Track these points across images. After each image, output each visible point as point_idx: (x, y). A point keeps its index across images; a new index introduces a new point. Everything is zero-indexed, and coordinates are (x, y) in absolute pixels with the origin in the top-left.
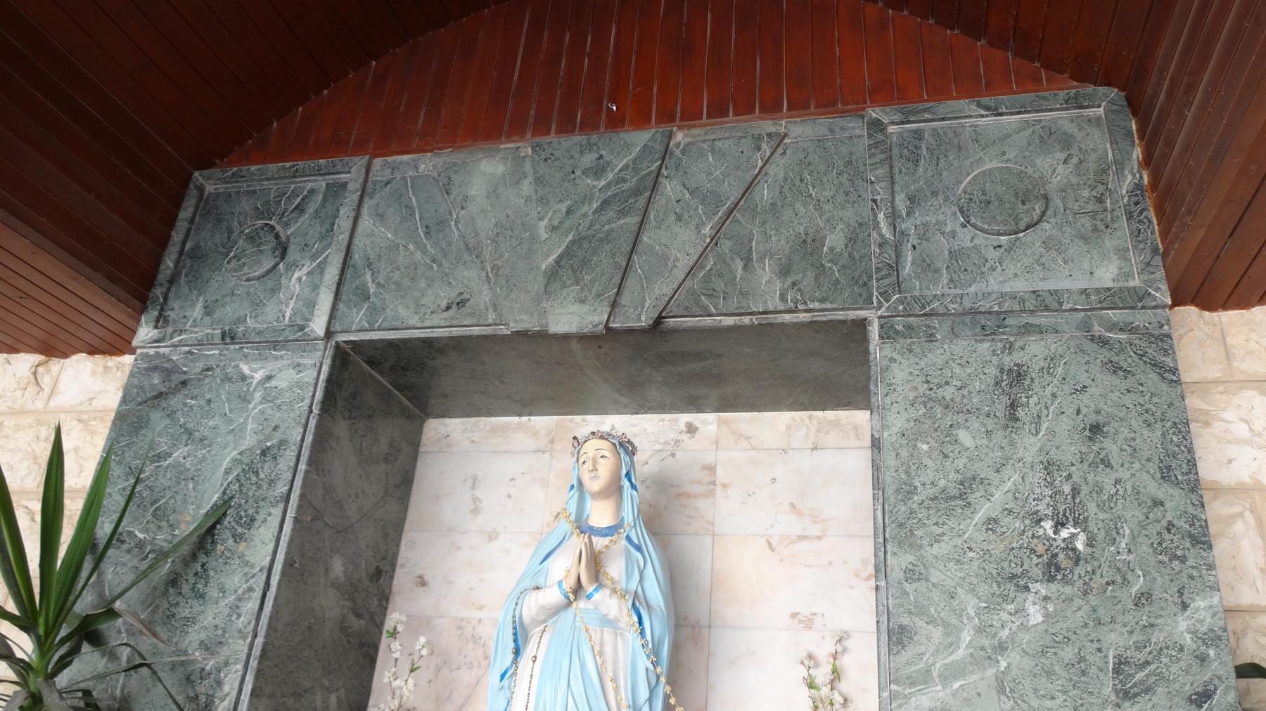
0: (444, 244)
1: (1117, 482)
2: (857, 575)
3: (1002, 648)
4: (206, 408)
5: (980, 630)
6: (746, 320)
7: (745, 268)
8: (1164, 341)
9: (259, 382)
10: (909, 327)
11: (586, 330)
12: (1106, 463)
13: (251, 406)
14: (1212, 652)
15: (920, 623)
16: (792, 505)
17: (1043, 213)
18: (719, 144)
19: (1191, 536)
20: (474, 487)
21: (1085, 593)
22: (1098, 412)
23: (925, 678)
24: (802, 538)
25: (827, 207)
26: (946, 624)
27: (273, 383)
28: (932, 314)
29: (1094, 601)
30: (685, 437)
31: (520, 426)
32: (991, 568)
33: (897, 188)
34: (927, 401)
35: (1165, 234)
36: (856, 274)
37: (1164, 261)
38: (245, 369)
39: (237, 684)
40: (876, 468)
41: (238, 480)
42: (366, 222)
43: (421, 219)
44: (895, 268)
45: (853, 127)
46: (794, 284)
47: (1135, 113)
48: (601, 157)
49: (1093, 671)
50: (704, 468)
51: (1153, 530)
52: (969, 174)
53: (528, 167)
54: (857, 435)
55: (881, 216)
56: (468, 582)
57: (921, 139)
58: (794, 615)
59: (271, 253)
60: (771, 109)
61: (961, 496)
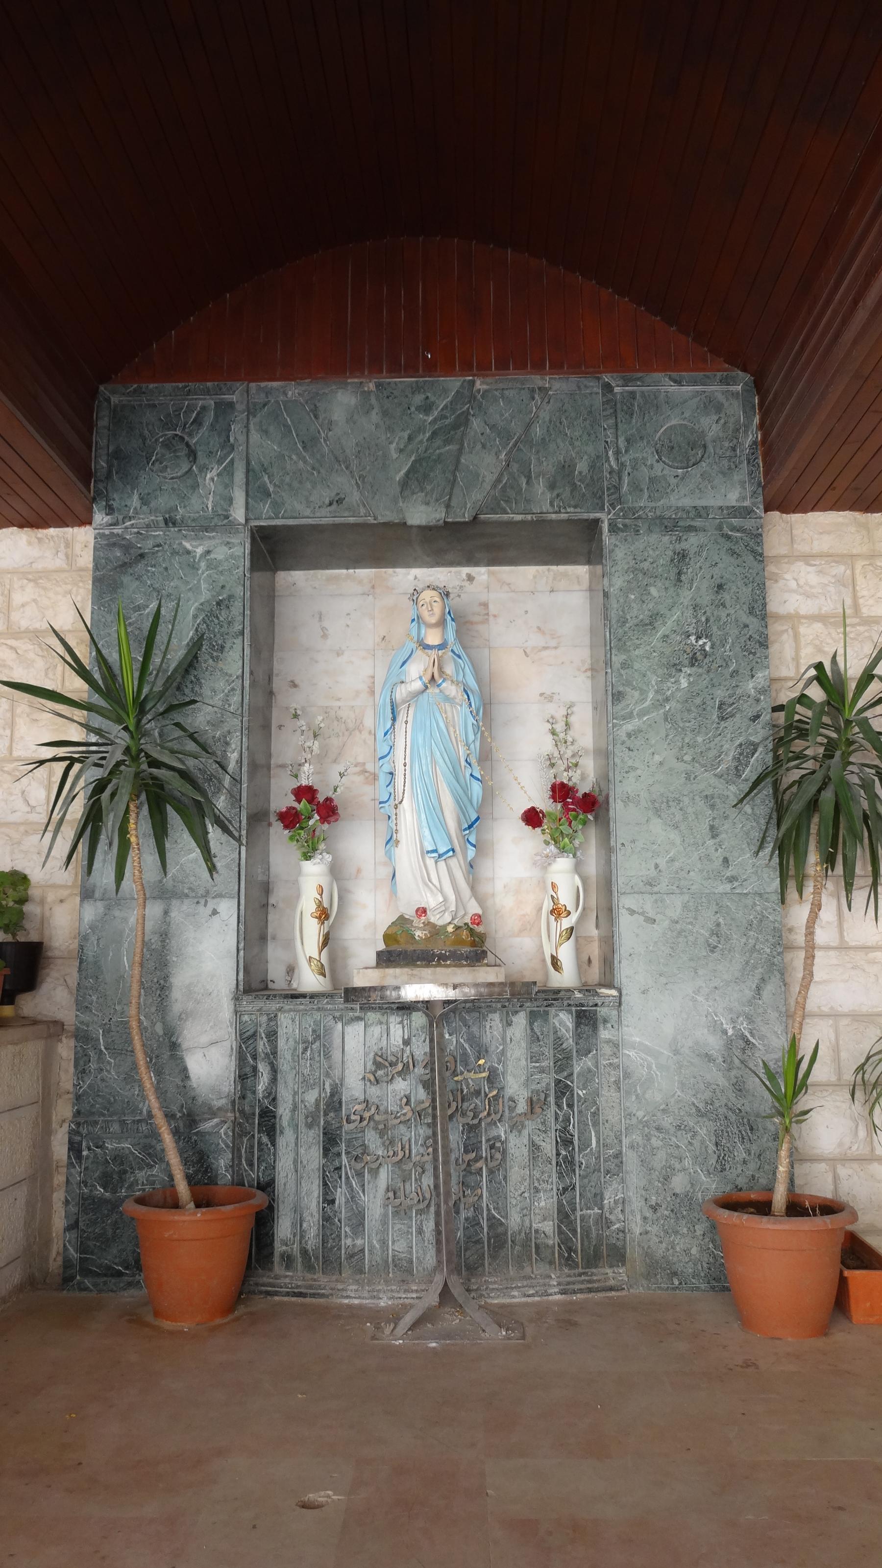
0: (319, 457)
1: (728, 615)
2: (579, 670)
3: (667, 700)
4: (165, 574)
5: (657, 692)
6: (529, 517)
7: (527, 483)
8: (757, 536)
9: (201, 556)
10: (625, 526)
12: (723, 605)
13: (200, 572)
14: (762, 697)
15: (628, 689)
16: (539, 628)
17: (703, 456)
18: (506, 392)
19: (760, 642)
21: (708, 672)
22: (722, 578)
23: (630, 716)
24: (545, 648)
25: (577, 443)
26: (641, 690)
27: (212, 556)
28: (639, 518)
29: (712, 675)
30: (467, 584)
31: (348, 577)
32: (664, 661)
33: (619, 433)
34: (634, 570)
35: (766, 474)
36: (595, 490)
37: (763, 491)
38: (188, 545)
39: (239, 743)
40: (606, 608)
41: (205, 622)
42: (255, 436)
43: (297, 435)
44: (617, 488)
45: (592, 386)
46: (558, 495)
47: (758, 393)
48: (427, 398)
49: (709, 708)
50: (480, 604)
51: (742, 640)
52: (662, 427)
53: (373, 401)
54: (579, 582)
55: (610, 453)
57: (634, 398)
58: (542, 694)
59: (186, 459)
60: (538, 367)
61: (651, 624)
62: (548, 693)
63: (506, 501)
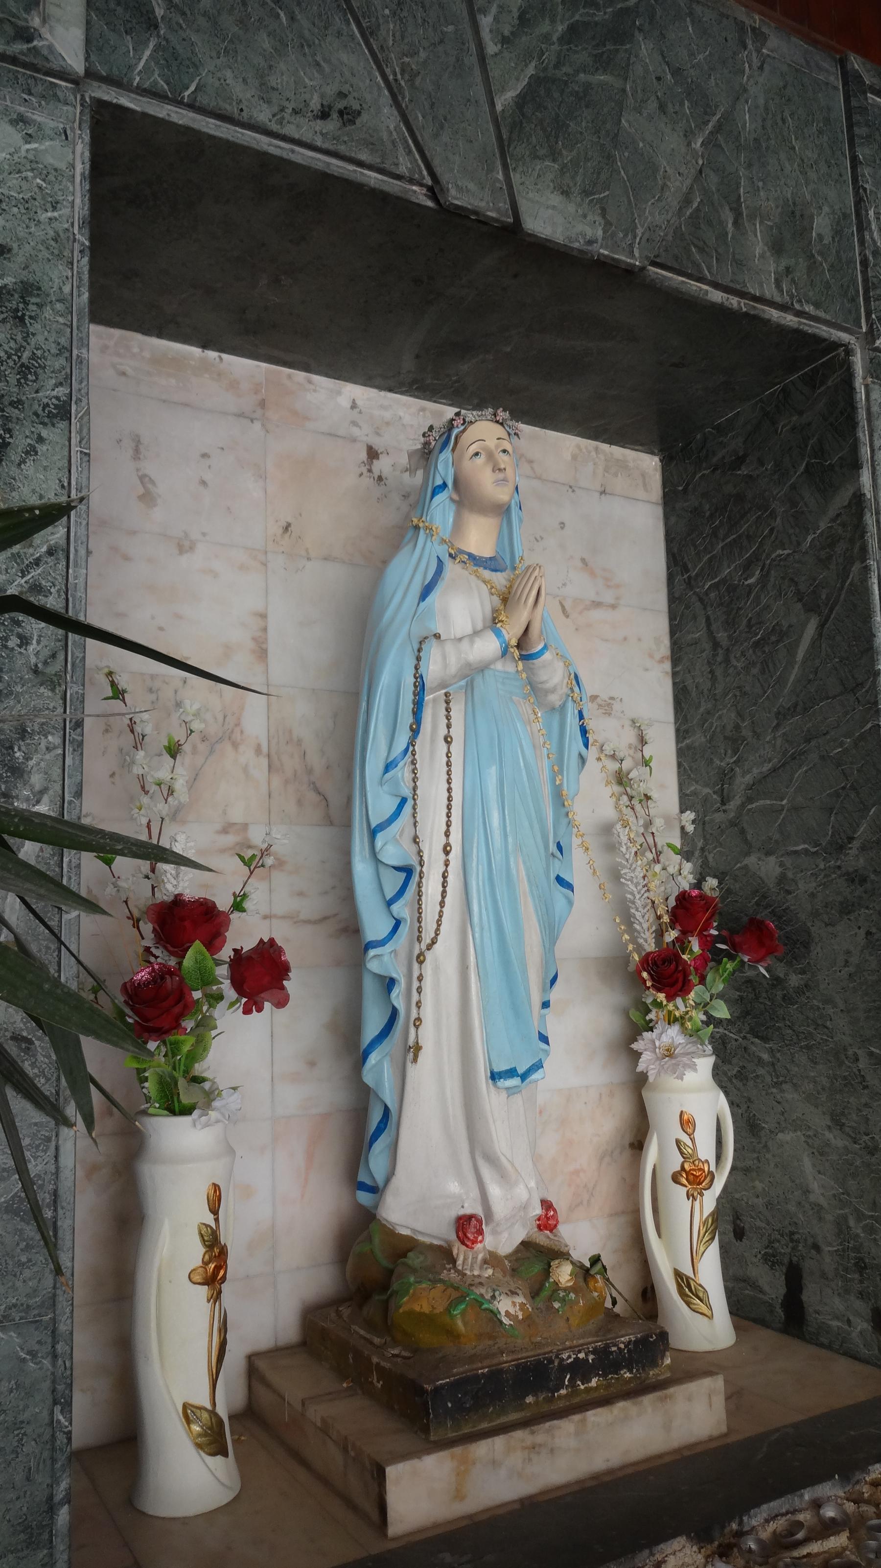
2: (651, 656)
7: (736, 223)
11: (576, 245)
16: (583, 560)
20: (137, 454)
24: (597, 605)
31: (205, 367)
39: (56, 772)
56: (153, 618)
62: (604, 696)
63: (701, 250)
